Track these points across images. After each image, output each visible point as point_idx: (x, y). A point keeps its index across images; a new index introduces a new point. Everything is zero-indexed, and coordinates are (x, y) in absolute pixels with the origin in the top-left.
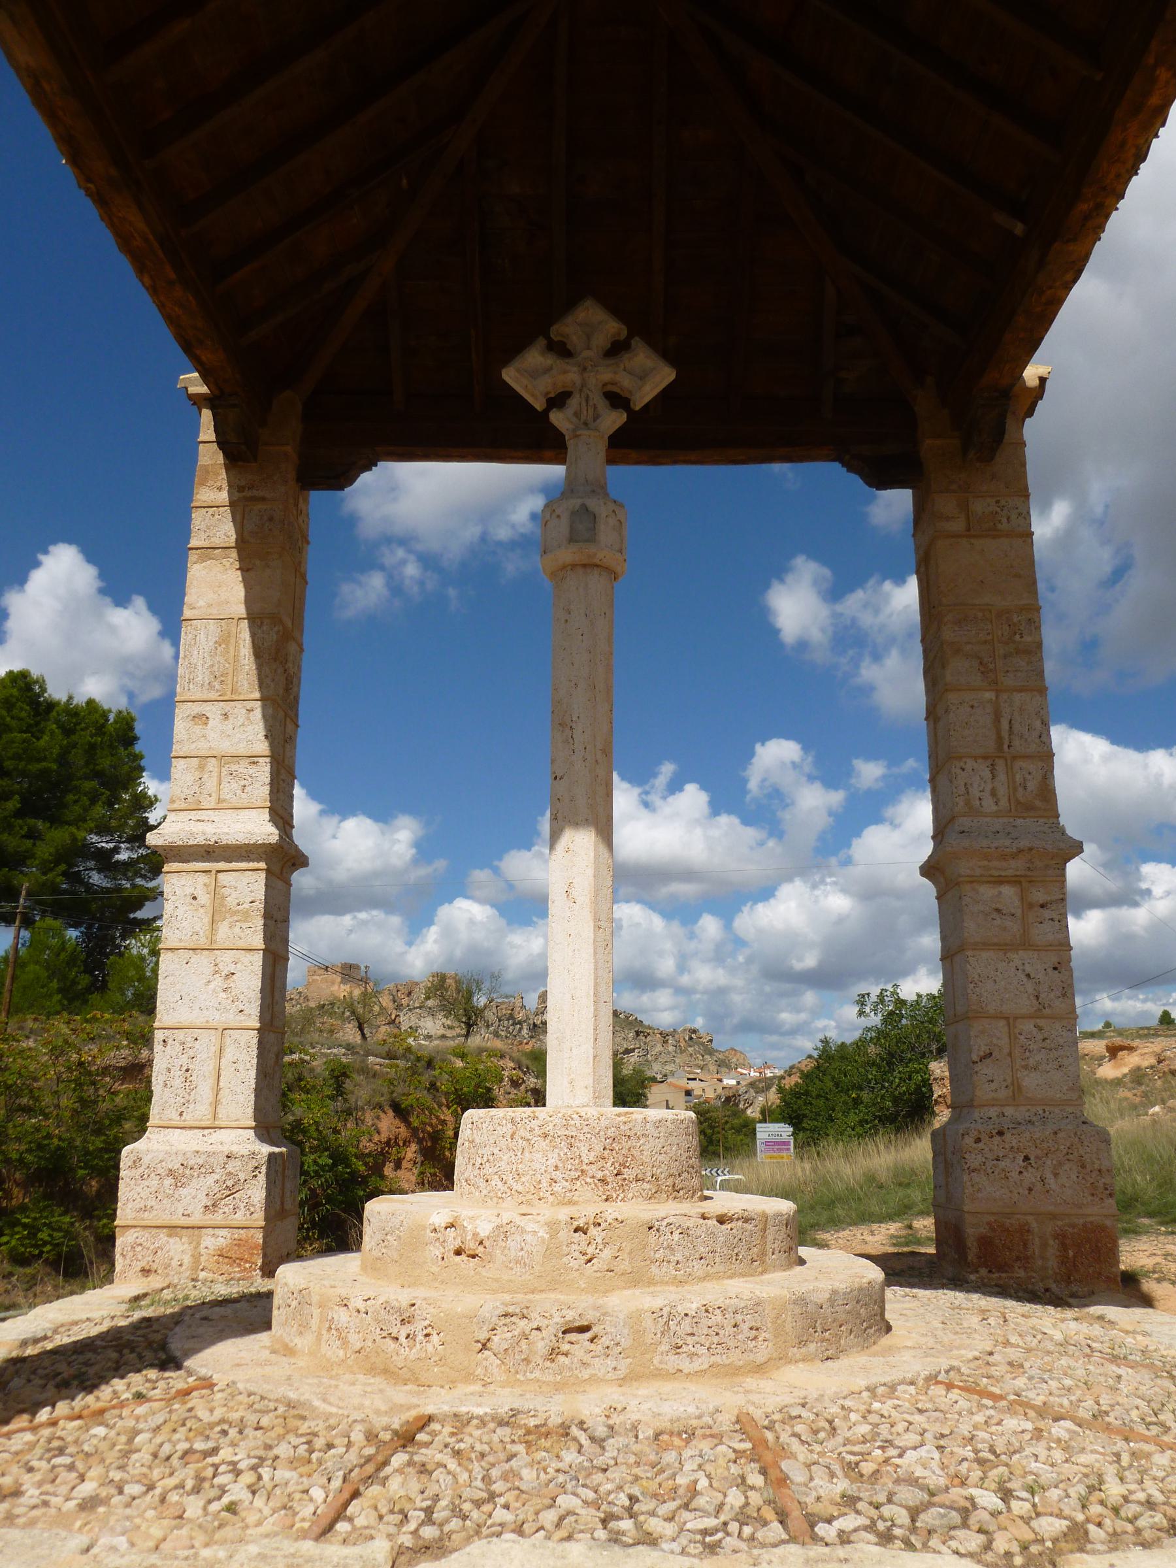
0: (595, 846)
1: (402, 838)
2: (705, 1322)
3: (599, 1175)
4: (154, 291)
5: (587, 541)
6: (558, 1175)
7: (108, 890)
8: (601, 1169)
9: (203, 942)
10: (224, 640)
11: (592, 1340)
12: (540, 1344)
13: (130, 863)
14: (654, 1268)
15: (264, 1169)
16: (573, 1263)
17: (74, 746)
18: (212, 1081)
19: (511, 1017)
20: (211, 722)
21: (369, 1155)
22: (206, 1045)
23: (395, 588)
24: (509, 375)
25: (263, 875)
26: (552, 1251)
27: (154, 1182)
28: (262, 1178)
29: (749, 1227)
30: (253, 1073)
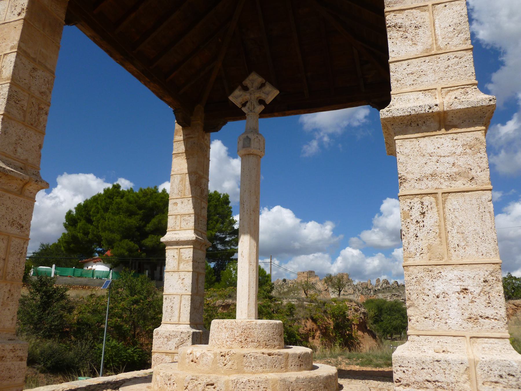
0: (250, 240)
1: (328, 228)
2: (248, 385)
3: (240, 340)
4: (146, 85)
5: (247, 147)
6: (228, 340)
7: (222, 250)
8: (241, 338)
9: (176, 269)
10: (182, 180)
11: (214, 388)
12: (200, 388)
13: (229, 242)
14: (245, 368)
15: (191, 336)
16: (220, 366)
17: (211, 205)
18: (178, 310)
19: (367, 287)
20: (178, 205)
21: (303, 334)
22: (177, 299)
23: (321, 145)
24: (231, 98)
25: (192, 249)
26: (215, 362)
27: (162, 339)
28: (191, 339)
29: (280, 357)
30: (189, 308)
